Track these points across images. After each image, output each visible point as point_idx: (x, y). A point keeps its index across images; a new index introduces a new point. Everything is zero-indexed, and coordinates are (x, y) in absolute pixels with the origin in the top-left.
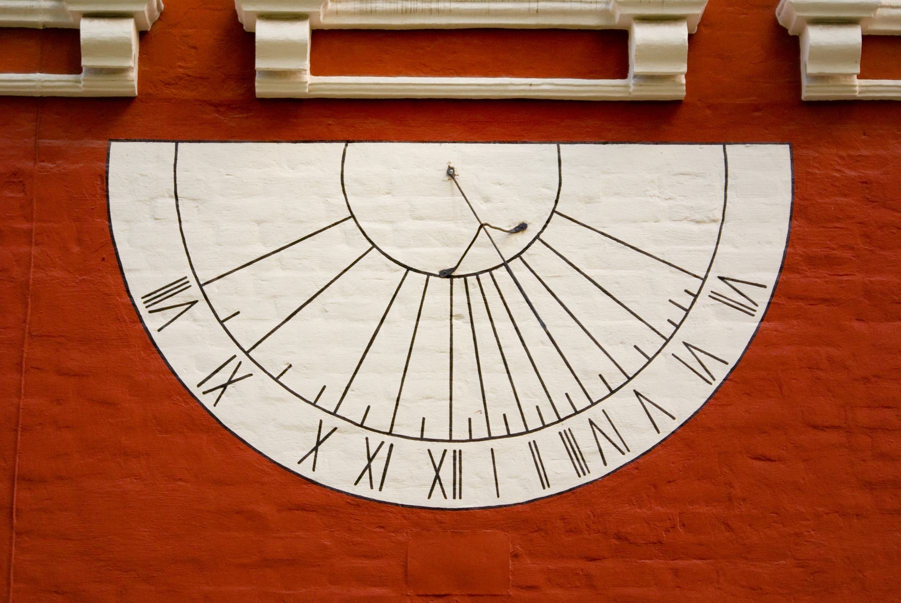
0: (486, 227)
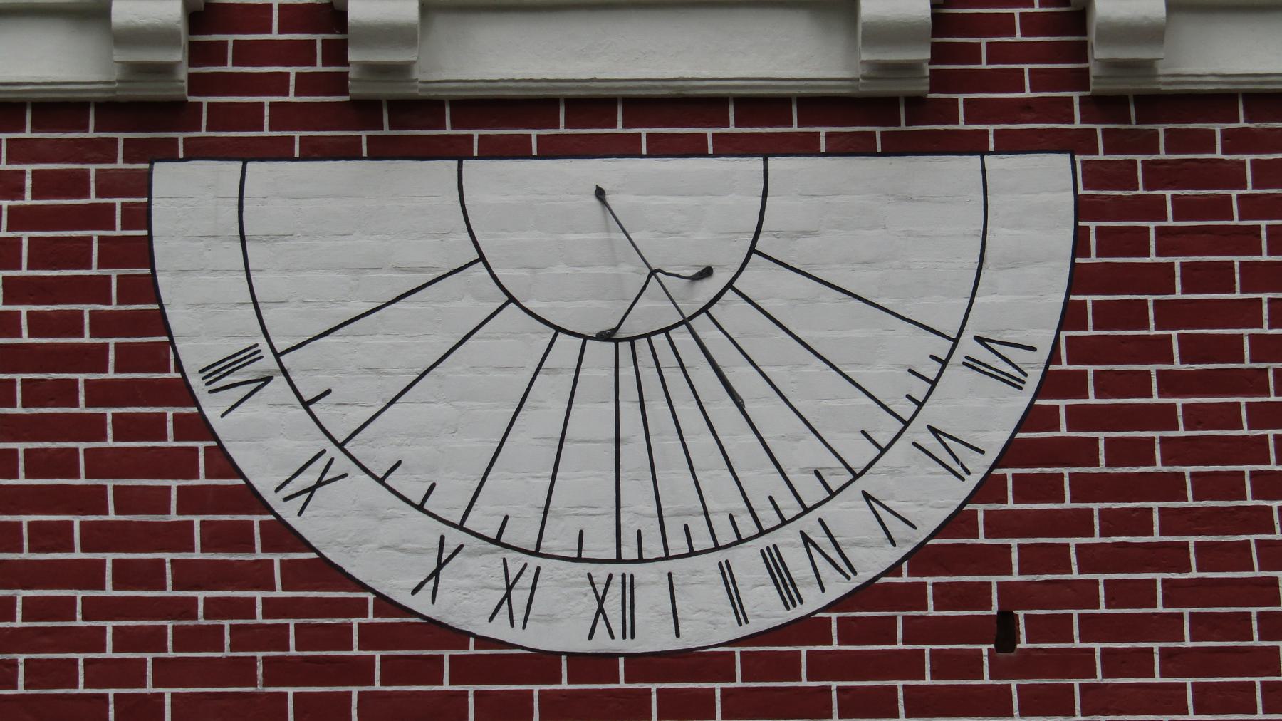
0: (659, 274)
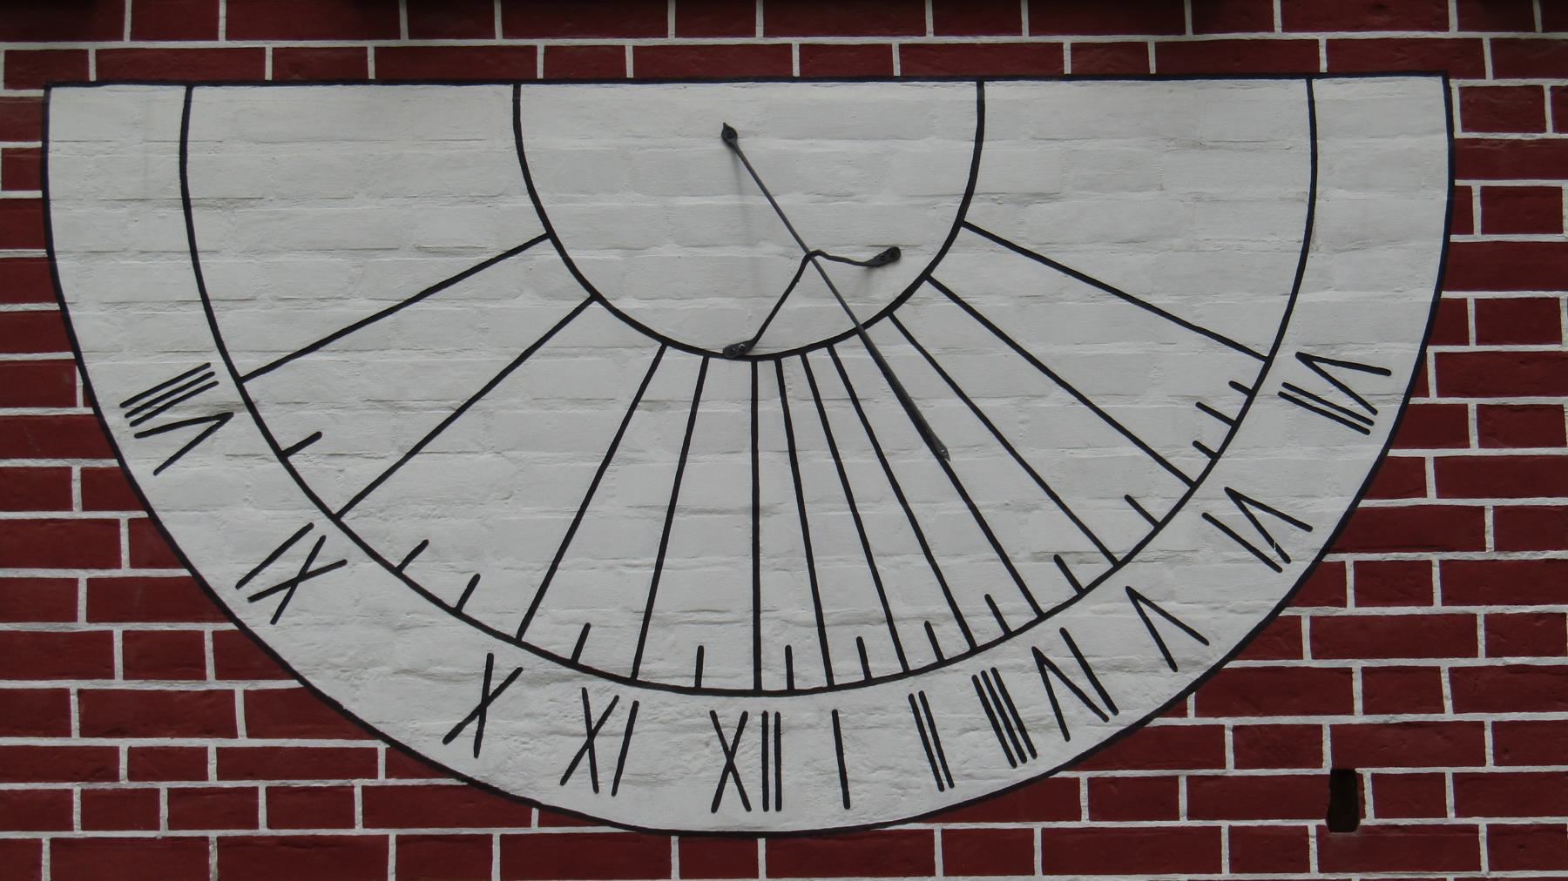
0: (818, 258)
